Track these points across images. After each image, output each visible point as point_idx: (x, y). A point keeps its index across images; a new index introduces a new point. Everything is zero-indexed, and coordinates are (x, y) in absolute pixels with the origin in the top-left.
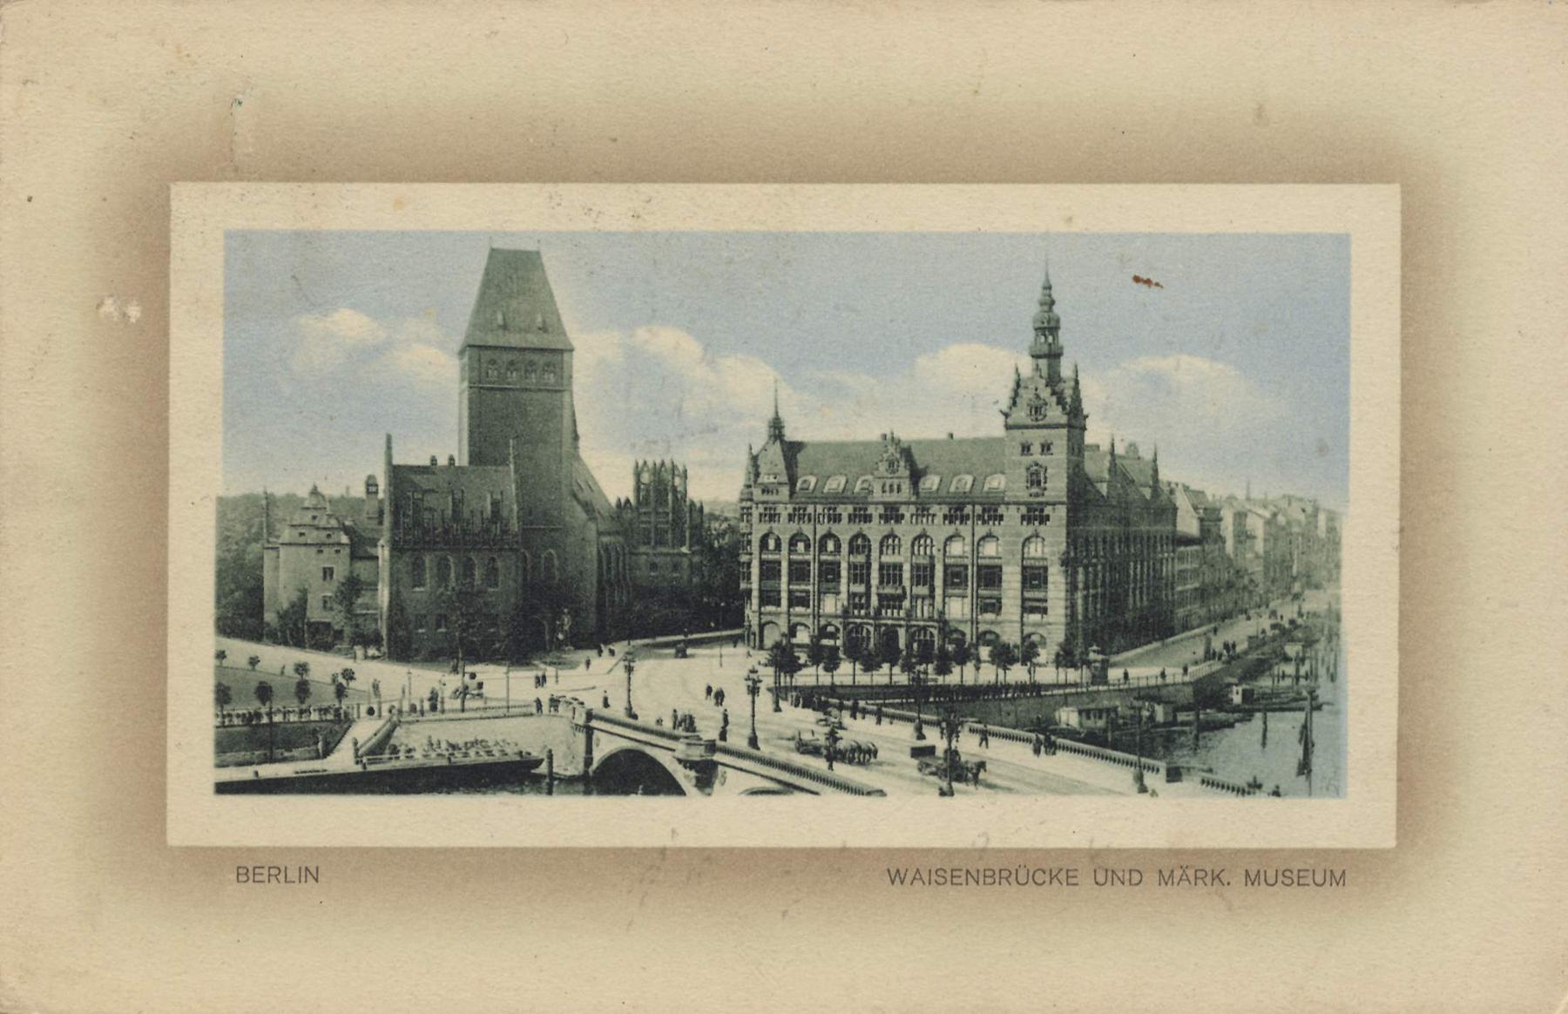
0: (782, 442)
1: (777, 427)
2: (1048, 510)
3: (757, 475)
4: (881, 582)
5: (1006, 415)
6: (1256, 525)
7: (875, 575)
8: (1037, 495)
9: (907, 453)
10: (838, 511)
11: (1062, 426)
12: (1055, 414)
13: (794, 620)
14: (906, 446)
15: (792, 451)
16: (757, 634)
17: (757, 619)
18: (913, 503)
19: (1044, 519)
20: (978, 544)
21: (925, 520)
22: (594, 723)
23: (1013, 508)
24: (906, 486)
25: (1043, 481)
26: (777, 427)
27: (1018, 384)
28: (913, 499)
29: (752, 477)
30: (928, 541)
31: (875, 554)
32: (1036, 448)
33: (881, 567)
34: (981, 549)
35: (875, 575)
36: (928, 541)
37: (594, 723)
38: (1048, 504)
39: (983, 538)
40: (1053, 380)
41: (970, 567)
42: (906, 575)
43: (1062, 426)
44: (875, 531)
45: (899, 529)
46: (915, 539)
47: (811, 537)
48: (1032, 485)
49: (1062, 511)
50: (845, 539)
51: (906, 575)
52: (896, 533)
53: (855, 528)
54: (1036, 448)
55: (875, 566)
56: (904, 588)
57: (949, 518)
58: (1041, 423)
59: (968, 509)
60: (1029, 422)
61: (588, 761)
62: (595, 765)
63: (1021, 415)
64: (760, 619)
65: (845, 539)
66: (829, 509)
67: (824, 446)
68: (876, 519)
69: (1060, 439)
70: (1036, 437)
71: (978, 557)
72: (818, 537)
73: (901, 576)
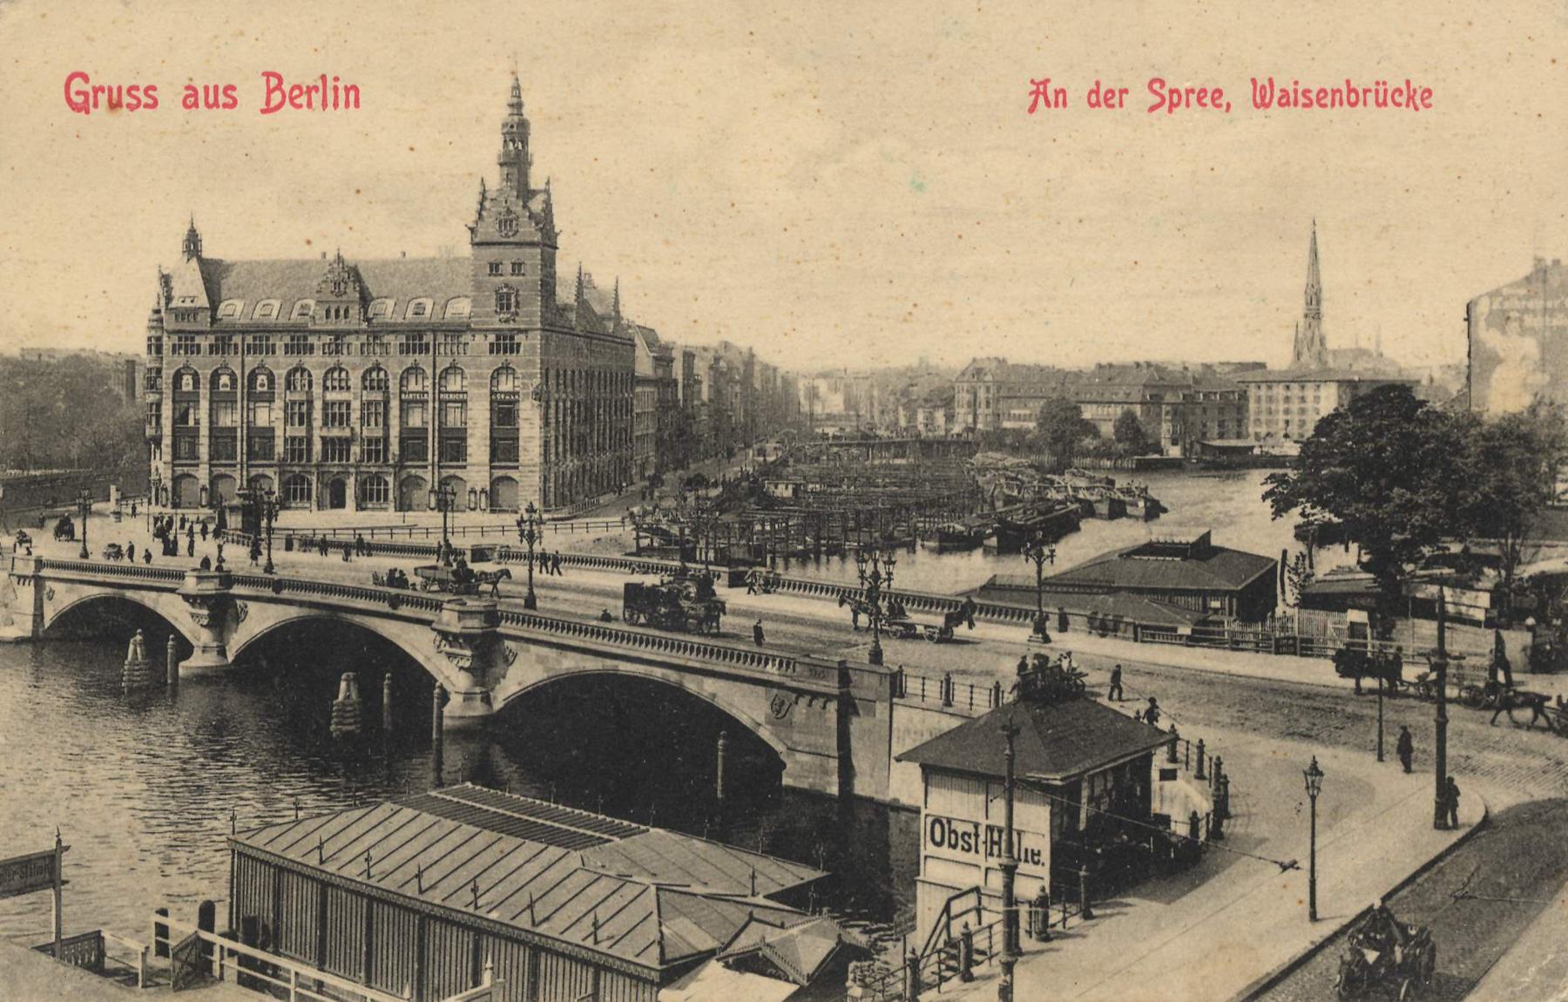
0: (201, 261)
1: (193, 243)
2: (518, 338)
3: (169, 299)
4: (325, 424)
5: (472, 230)
6: (701, 368)
7: (317, 414)
8: (507, 321)
9: (354, 274)
10: (196, 342)
11: (532, 244)
12: (529, 231)
13: (217, 470)
14: (352, 265)
15: (213, 274)
16: (170, 489)
17: (170, 472)
18: (365, 332)
19: (514, 348)
20: (440, 378)
21: (455, 349)
22: (45, 572)
23: (479, 338)
24: (355, 311)
25: (513, 305)
26: (193, 243)
27: (484, 198)
28: (364, 326)
29: (163, 302)
30: (343, 375)
31: (317, 390)
32: (507, 268)
33: (326, 405)
34: (443, 382)
35: (317, 414)
36: (343, 375)
37: (45, 572)
38: (520, 331)
39: (446, 370)
40: (526, 194)
41: (239, 430)
42: (355, 415)
43: (532, 244)
44: (316, 363)
45: (309, 361)
46: (326, 373)
47: (238, 372)
48: (501, 309)
49: (536, 339)
50: (280, 374)
51: (355, 415)
52: (306, 366)
53: (293, 361)
54: (507, 268)
55: (318, 405)
56: (352, 429)
57: (405, 349)
58: (511, 240)
59: (237, 339)
60: (497, 237)
61: (38, 615)
62: (47, 623)
63: (490, 230)
64: (173, 471)
65: (280, 374)
66: (186, 339)
67: (252, 267)
68: (280, 351)
69: (533, 256)
70: (508, 256)
71: (440, 392)
72: (247, 372)
73: (348, 415)
